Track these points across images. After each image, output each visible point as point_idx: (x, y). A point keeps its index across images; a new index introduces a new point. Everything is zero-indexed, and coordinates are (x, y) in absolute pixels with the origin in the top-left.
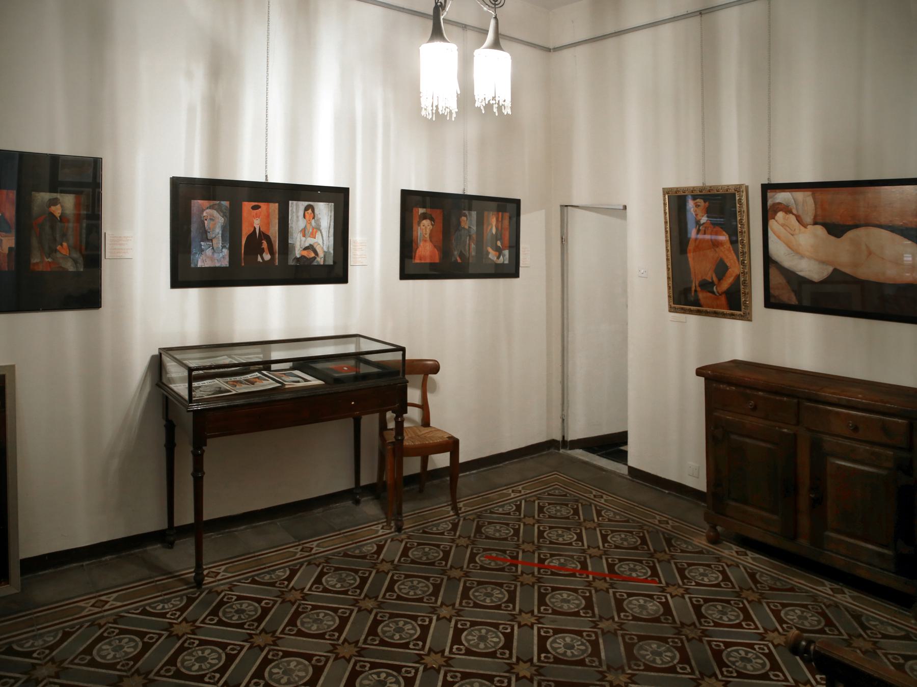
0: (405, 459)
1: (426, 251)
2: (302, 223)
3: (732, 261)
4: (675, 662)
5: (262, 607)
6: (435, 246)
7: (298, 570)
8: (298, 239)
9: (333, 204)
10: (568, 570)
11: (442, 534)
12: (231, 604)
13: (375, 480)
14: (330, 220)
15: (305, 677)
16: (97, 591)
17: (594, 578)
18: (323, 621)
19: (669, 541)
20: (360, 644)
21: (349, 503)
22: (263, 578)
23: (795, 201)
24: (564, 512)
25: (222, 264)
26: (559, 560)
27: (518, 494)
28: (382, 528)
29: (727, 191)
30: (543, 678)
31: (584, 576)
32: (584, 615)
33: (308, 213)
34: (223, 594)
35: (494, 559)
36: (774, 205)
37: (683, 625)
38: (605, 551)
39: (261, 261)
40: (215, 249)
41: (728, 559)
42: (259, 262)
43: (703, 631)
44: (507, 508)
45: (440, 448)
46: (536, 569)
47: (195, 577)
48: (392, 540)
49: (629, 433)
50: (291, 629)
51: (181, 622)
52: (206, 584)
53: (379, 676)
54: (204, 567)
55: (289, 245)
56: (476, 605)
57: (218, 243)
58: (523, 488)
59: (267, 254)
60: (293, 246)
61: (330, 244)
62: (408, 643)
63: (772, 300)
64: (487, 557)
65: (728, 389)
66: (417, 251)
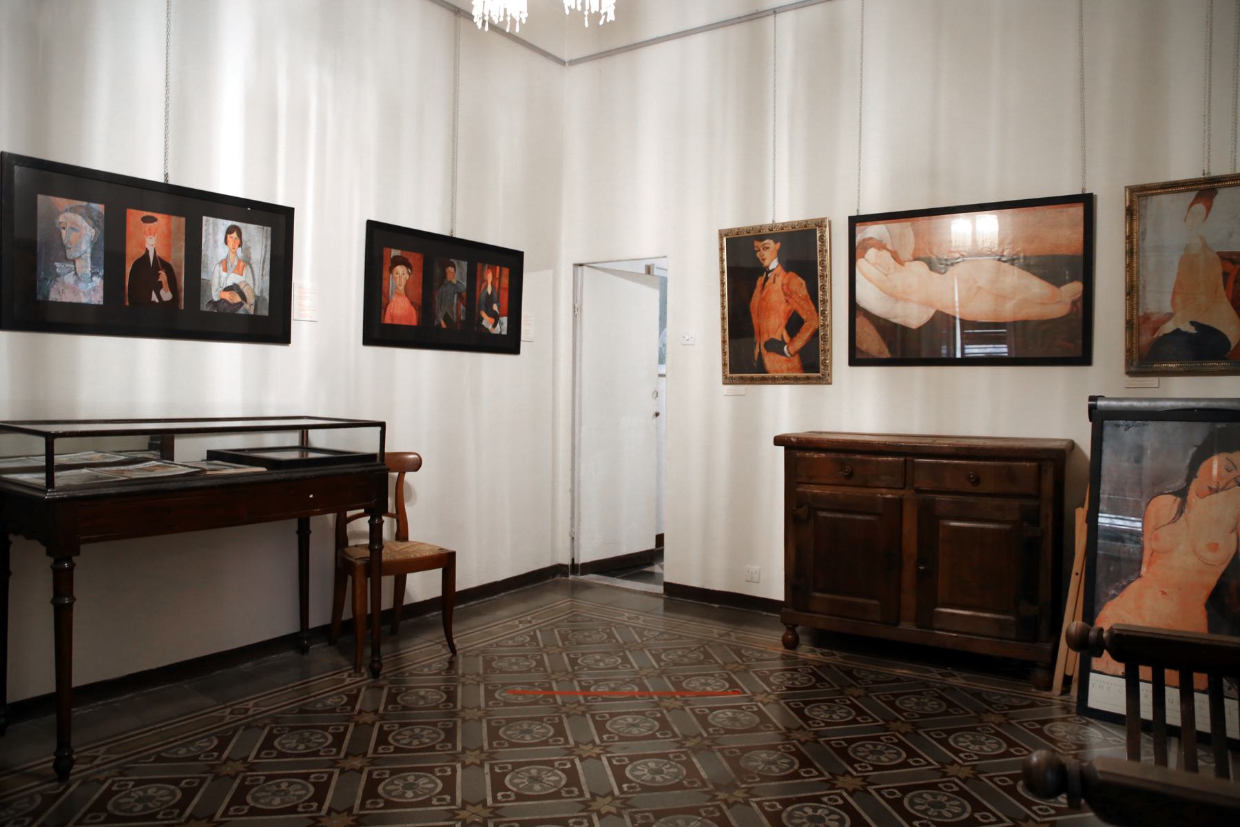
1: (400, 309)
2: (222, 251)
3: (809, 313)
4: (796, 767)
6: (412, 303)
8: (217, 274)
9: (270, 229)
10: (625, 694)
12: (127, 792)
13: (328, 621)
14: (266, 252)
18: (289, 792)
20: (355, 811)
23: (890, 235)
25: (91, 300)
28: (349, 676)
29: (806, 227)
30: (634, 810)
32: (566, 795)
33: (231, 237)
34: (109, 782)
35: (522, 693)
36: (864, 240)
39: (157, 301)
40: (79, 274)
42: (154, 302)
43: (816, 733)
46: (581, 698)
50: (239, 809)
52: (74, 774)
55: (202, 281)
56: (512, 745)
57: (85, 266)
58: (533, 618)
59: (167, 291)
60: (209, 283)
61: (264, 285)
62: (430, 799)
63: (859, 356)
65: (816, 456)
66: (388, 308)
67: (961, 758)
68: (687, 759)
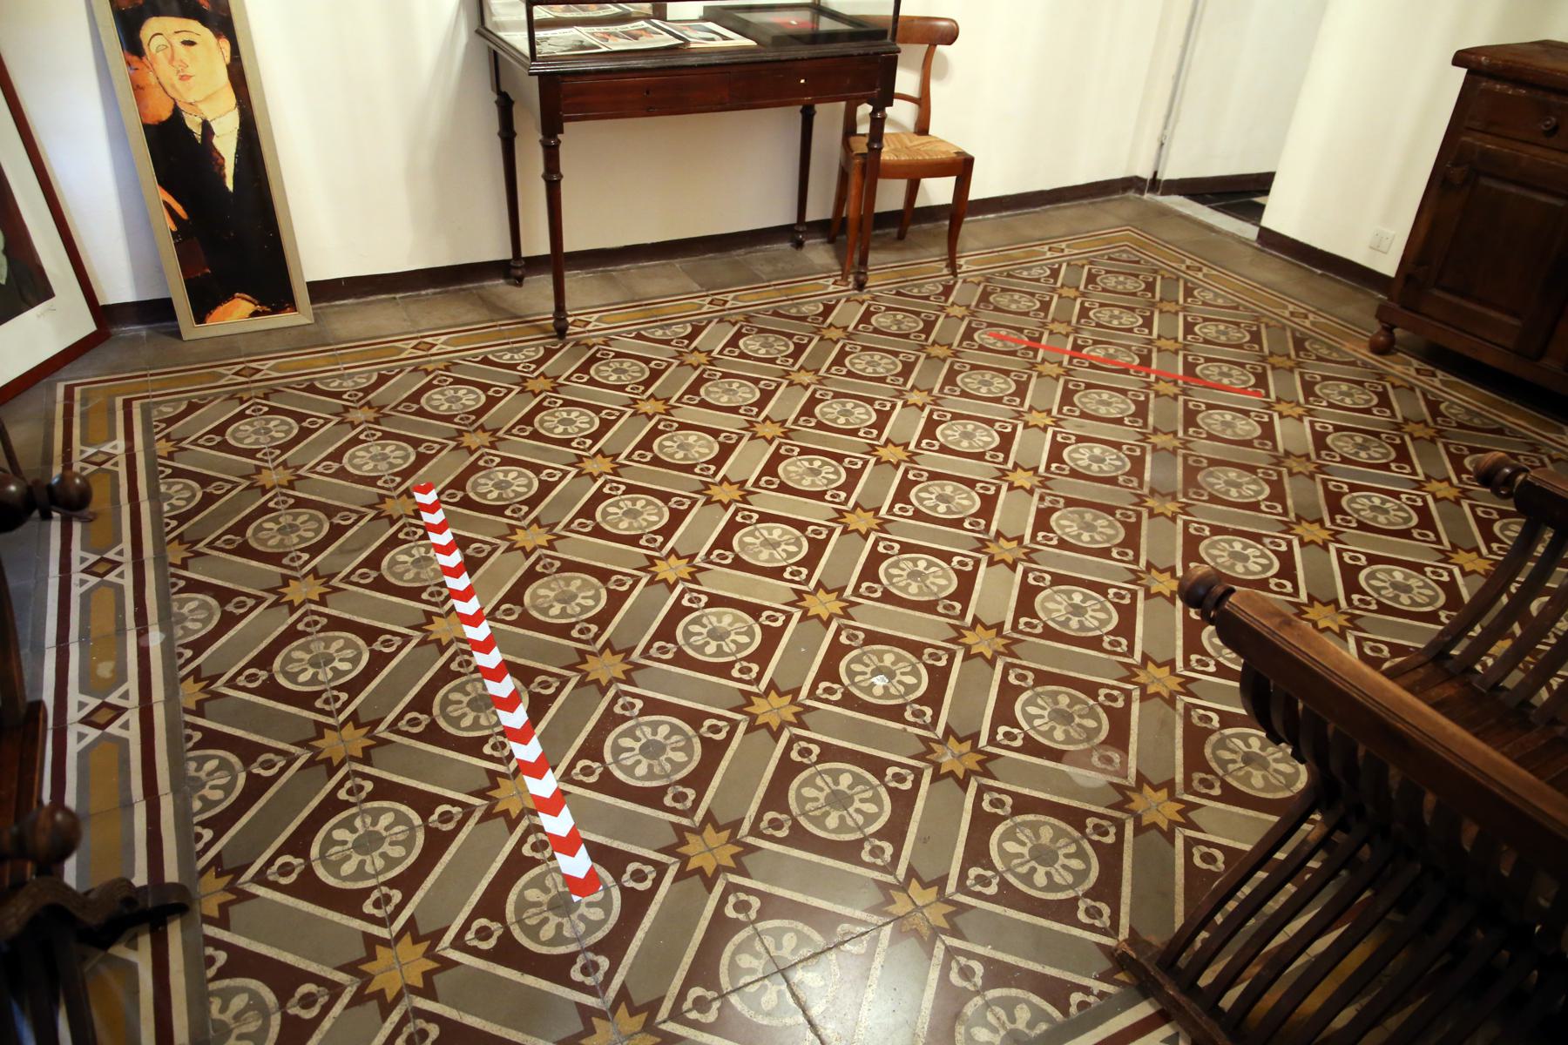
0: (881, 182)
5: (651, 369)
7: (704, 328)
11: (927, 298)
13: (828, 215)
15: (684, 765)
16: (419, 332)
17: (1157, 380)
19: (1299, 344)
21: (786, 246)
22: (653, 333)
24: (1131, 285)
26: (1106, 349)
28: (834, 283)
31: (1143, 374)
34: (595, 348)
35: (1001, 338)
37: (1287, 454)
38: (1185, 345)
41: (1397, 377)
44: (1035, 273)
45: (939, 169)
46: (1066, 359)
47: (554, 324)
48: (848, 300)
49: (1276, 177)
51: (537, 377)
53: (811, 464)
54: (570, 320)
64: (991, 335)
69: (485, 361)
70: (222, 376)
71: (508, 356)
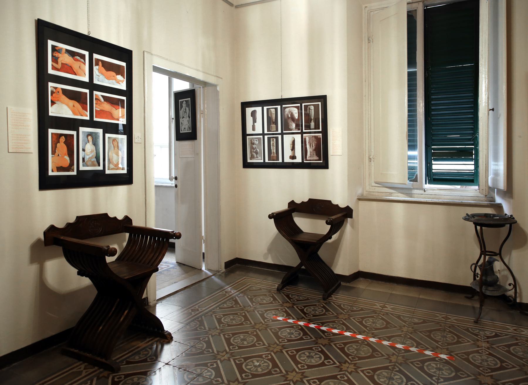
27: (197, 312)
58: (199, 307)
67: (345, 312)
68: (271, 357)
69: (467, 330)
70: (391, 308)
71: (478, 331)
